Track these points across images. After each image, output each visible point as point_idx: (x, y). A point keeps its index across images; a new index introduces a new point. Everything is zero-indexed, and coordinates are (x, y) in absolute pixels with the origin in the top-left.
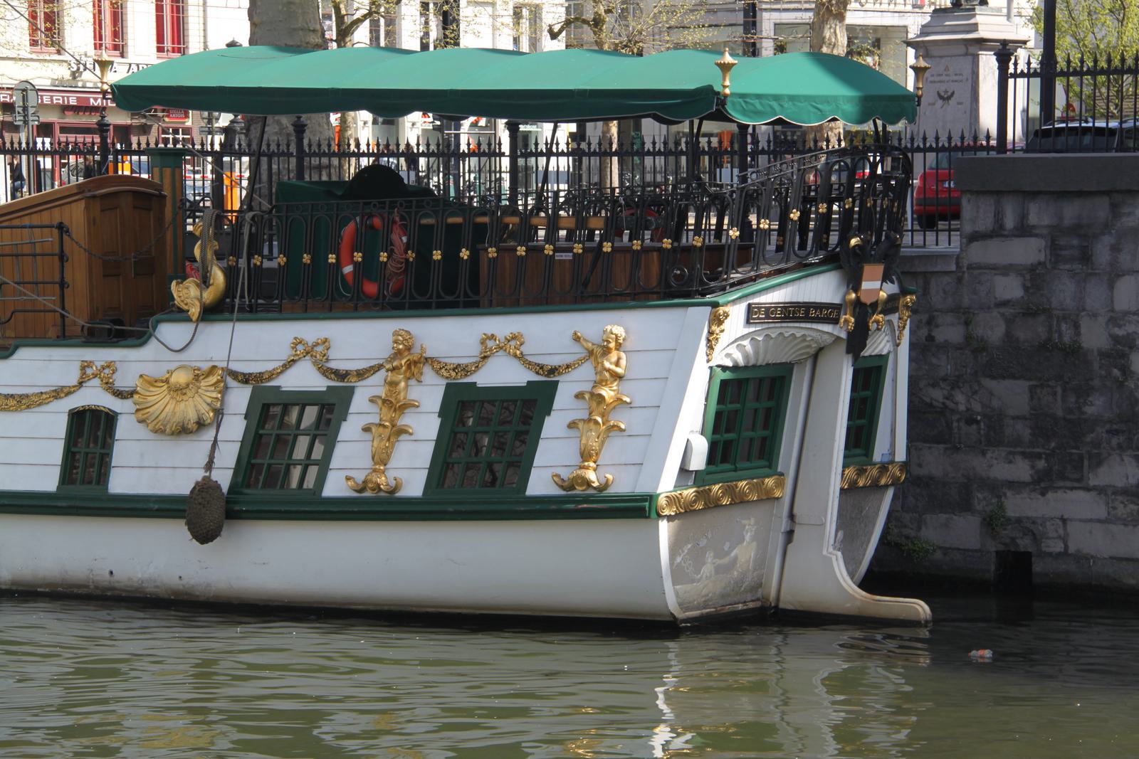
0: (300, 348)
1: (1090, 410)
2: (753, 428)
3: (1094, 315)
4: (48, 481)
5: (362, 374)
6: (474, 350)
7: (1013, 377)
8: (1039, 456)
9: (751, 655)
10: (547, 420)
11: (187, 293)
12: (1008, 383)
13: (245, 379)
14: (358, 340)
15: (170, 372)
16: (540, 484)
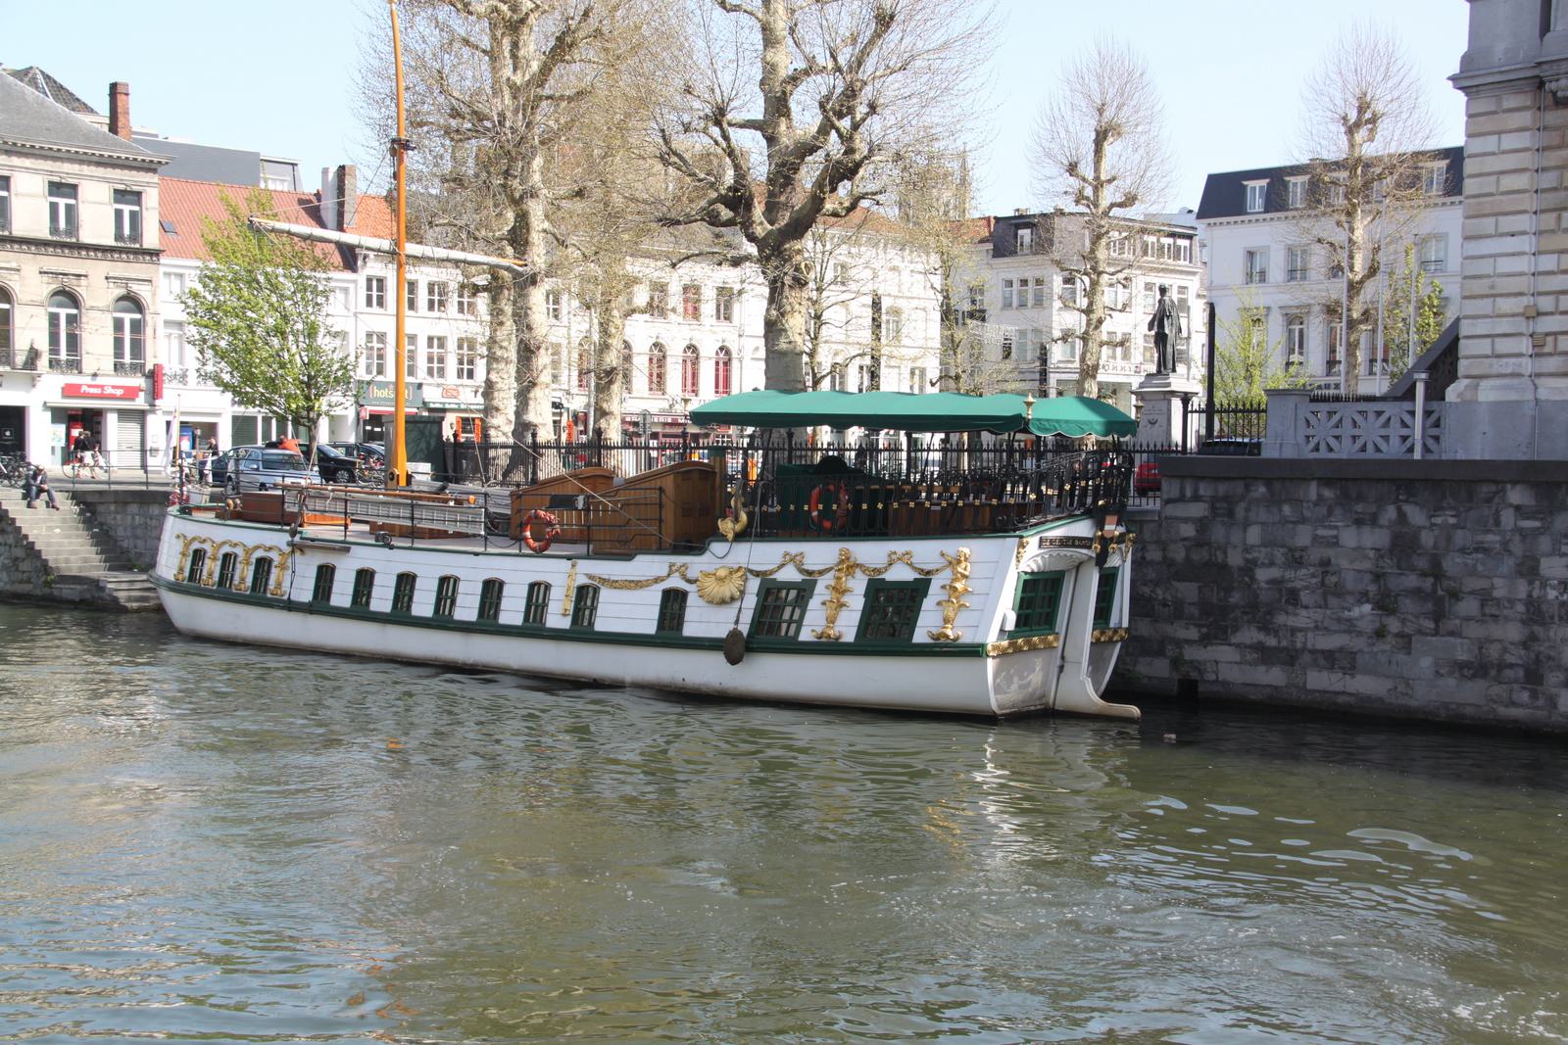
5: (821, 573)
11: (727, 526)
13: (757, 574)
14: (820, 554)
16: (920, 636)
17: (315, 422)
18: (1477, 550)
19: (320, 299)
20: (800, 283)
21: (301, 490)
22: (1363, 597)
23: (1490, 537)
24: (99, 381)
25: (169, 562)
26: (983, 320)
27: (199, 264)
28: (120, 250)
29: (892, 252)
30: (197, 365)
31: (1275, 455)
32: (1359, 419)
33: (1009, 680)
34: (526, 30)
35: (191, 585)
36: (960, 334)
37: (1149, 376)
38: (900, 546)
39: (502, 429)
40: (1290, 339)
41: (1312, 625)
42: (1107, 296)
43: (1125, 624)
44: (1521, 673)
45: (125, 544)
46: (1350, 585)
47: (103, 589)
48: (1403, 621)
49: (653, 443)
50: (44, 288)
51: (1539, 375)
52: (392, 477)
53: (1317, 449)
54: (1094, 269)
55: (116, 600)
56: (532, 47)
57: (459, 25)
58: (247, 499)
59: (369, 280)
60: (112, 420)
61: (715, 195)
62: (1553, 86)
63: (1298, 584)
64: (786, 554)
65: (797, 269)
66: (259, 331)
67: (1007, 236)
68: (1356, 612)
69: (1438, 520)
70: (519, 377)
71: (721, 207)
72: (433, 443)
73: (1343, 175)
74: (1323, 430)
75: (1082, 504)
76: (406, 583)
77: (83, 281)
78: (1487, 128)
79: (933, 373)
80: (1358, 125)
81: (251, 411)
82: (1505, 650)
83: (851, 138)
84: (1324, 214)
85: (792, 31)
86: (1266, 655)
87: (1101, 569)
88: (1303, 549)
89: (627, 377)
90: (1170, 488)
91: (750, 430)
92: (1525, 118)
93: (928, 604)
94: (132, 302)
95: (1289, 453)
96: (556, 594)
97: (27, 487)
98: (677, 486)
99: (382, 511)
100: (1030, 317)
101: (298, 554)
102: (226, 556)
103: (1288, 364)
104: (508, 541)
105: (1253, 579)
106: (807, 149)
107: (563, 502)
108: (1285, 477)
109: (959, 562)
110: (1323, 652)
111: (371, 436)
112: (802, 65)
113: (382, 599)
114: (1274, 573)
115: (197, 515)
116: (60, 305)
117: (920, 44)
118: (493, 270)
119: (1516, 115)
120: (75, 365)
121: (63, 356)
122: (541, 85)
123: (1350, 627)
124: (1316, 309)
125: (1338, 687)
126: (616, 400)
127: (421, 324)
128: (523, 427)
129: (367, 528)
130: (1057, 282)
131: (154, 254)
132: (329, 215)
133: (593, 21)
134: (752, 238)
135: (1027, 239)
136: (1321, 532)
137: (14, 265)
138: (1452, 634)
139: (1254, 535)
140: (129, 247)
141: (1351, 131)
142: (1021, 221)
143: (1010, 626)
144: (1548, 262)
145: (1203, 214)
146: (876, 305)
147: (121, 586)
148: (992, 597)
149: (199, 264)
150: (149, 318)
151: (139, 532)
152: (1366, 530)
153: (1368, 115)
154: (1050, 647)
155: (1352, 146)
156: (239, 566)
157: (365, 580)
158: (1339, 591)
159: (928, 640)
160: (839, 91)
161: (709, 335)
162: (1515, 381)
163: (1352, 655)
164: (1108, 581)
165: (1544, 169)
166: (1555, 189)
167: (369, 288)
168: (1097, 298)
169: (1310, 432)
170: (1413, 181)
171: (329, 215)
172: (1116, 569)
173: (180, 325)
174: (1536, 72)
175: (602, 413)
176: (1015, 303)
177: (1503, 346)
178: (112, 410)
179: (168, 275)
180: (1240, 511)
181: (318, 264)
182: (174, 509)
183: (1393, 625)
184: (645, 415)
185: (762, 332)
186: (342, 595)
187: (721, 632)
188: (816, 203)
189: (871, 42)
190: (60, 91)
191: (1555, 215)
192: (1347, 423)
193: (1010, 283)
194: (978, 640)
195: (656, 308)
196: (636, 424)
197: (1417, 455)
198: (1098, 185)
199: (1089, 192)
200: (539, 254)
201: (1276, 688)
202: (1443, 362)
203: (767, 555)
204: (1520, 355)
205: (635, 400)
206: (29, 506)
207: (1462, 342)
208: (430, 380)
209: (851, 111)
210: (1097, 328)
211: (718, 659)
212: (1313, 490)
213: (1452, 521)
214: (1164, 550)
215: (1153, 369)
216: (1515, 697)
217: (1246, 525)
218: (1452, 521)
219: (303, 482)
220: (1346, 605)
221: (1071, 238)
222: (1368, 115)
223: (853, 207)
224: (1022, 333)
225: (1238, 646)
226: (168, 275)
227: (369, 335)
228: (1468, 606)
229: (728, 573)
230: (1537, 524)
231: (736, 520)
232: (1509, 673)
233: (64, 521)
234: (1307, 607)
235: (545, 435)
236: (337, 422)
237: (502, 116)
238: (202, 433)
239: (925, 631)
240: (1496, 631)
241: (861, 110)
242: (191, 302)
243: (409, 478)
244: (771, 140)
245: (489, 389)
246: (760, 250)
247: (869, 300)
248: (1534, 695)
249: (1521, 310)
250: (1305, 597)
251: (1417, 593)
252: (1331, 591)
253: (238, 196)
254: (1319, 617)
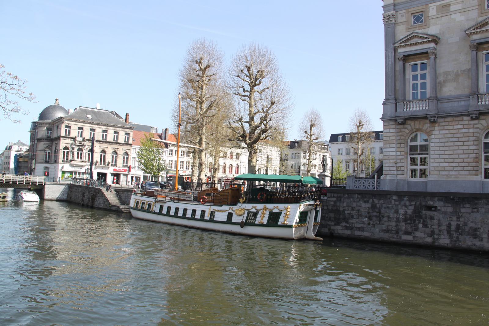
1: (340, 217)
5: (260, 210)
13: (247, 210)
14: (260, 206)
16: (280, 223)
17: (159, 177)
18: (387, 208)
19: (161, 154)
20: (255, 153)
21: (158, 190)
22: (366, 217)
23: (390, 206)
24: (120, 168)
25: (132, 204)
26: (288, 160)
27: (140, 147)
28: (125, 144)
29: (271, 147)
30: (138, 166)
31: (348, 189)
32: (364, 182)
33: (297, 232)
34: (203, 103)
35: (136, 208)
36: (284, 163)
37: (321, 172)
38: (276, 205)
39: (195, 180)
40: (347, 166)
42: (313, 156)
43: (320, 221)
44: (395, 232)
45: (124, 200)
46: (363, 214)
47: (120, 208)
48: (373, 222)
49: (223, 183)
50: (111, 151)
51: (397, 174)
52: (175, 188)
53: (356, 187)
54: (310, 151)
55: (122, 210)
56: (204, 107)
57: (190, 103)
58: (147, 192)
59: (170, 150)
60: (122, 176)
61: (239, 135)
62: (398, 121)
63: (353, 214)
64: (253, 206)
65: (255, 150)
66: (150, 159)
67: (293, 145)
68: (364, 220)
69: (380, 202)
70: (199, 170)
71: (240, 138)
72: (182, 182)
73: (356, 135)
74: (358, 184)
75: (312, 198)
76: (177, 209)
77: (118, 150)
78: (387, 128)
79: (278, 170)
80: (359, 126)
81: (147, 174)
82: (392, 227)
83: (266, 125)
84: (353, 142)
85: (255, 105)
86: (347, 228)
87: (316, 211)
88: (355, 207)
89: (219, 170)
90: (329, 195)
91: (242, 181)
92: (394, 126)
93: (281, 217)
94: (127, 153)
95: (351, 188)
96: (206, 213)
97: (107, 188)
98: (231, 192)
99: (173, 195)
100: (296, 161)
101: (156, 203)
102: (143, 203)
103: (346, 171)
104: (196, 202)
105: (345, 213)
106: (257, 127)
107: (208, 195)
108: (351, 193)
109: (288, 209)
110: (358, 227)
111: (169, 180)
112: (257, 111)
113: (172, 212)
114: (349, 212)
115: (138, 195)
116: (114, 154)
117: (279, 108)
118: (194, 149)
119: (392, 126)
120: (116, 165)
121: (114, 163)
122: (206, 114)
123: (363, 223)
124: (352, 160)
125: (361, 234)
126: (217, 174)
127: (181, 159)
128: (199, 179)
129: (170, 198)
130: (302, 154)
131: (131, 145)
132: (163, 138)
133: (216, 102)
134: (246, 144)
135: (297, 145)
136: (358, 204)
137: (107, 147)
138: (382, 224)
139: (345, 204)
140: (127, 143)
141: (358, 127)
142: (295, 142)
143: (298, 222)
144: (399, 153)
145: (330, 142)
146: (268, 157)
147: (123, 208)
148: (294, 216)
149: (140, 147)
150: (129, 157)
151: (126, 197)
152: (367, 203)
153: (361, 124)
154: (305, 226)
155: (358, 130)
156: (145, 205)
157: (169, 208)
158: (361, 216)
160: (264, 116)
161: (234, 162)
162: (393, 176)
163: (363, 228)
164: (317, 213)
165: (397, 136)
166: (399, 140)
167: (170, 152)
168: (311, 157)
169: (355, 184)
170: (369, 137)
171: (163, 138)
172: (318, 211)
173: (135, 158)
174: (395, 118)
175: (214, 177)
176: (294, 158)
177: (391, 169)
178: (122, 174)
179: (133, 148)
180: (342, 199)
181: (161, 147)
182: (133, 193)
183: (371, 222)
184: (222, 177)
185: (247, 162)
186: (165, 211)
187: (240, 221)
188: (259, 137)
189: (270, 107)
190: (117, 115)
191: (399, 144)
192: (362, 183)
193: (293, 154)
194: (291, 224)
195: (225, 157)
196: (220, 179)
197: (375, 189)
198: (311, 136)
199: (309, 137)
200: (204, 146)
201: (348, 234)
202: (380, 171)
203: (249, 206)
204: (394, 171)
205: (220, 175)
206: (107, 192)
207: (383, 168)
208: (180, 170)
209: (266, 120)
210: (310, 163)
211: (239, 227)
212: (356, 196)
213: (383, 202)
214: (327, 207)
215: (322, 171)
216: (394, 237)
217: (344, 202)
218: (383, 202)
219: (157, 189)
221: (305, 146)
222: (361, 124)
223: (266, 138)
224: (295, 163)
225: (341, 226)
226: (133, 148)
227: (169, 161)
228: (385, 219)
229: (242, 209)
230: (398, 203)
231: (243, 199)
232: (393, 232)
233: (113, 195)
234: (355, 219)
235: (204, 181)
236: (163, 177)
237: (198, 119)
238: (138, 179)
239: (280, 222)
240: (391, 224)
241: (268, 120)
242: (137, 154)
243: (178, 189)
244: (250, 125)
245: (193, 172)
246: (247, 146)
247: (266, 156)
248: (397, 236)
250: (355, 217)
251: (376, 216)
252: (360, 216)
253: (147, 134)
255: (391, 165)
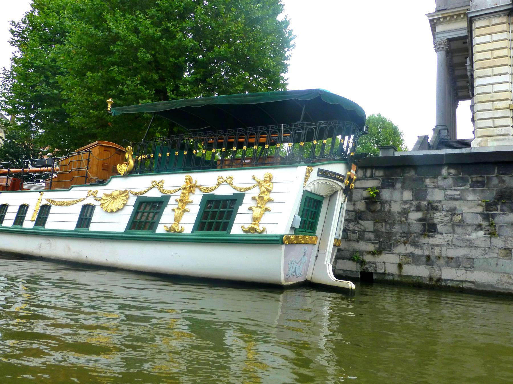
0: (154, 183)
2: (310, 218)
3: (396, 202)
4: (72, 226)
6: (216, 182)
7: (368, 220)
8: (377, 243)
9: (449, 301)
10: (240, 207)
11: (122, 168)
12: (367, 222)
13: (135, 194)
14: (173, 181)
15: (112, 192)
16: (236, 230)
22: (480, 227)
41: (445, 243)
68: (474, 236)
96: (30, 210)
123: (471, 244)
125: (462, 278)
158: (462, 223)
159: (241, 232)
163: (471, 260)
177: (498, 122)
183: (498, 242)
203: (144, 184)
204: (509, 126)
214: (354, 205)
220: (467, 232)
234: (441, 234)
249: (508, 106)
254: (450, 239)
255: (499, 114)
